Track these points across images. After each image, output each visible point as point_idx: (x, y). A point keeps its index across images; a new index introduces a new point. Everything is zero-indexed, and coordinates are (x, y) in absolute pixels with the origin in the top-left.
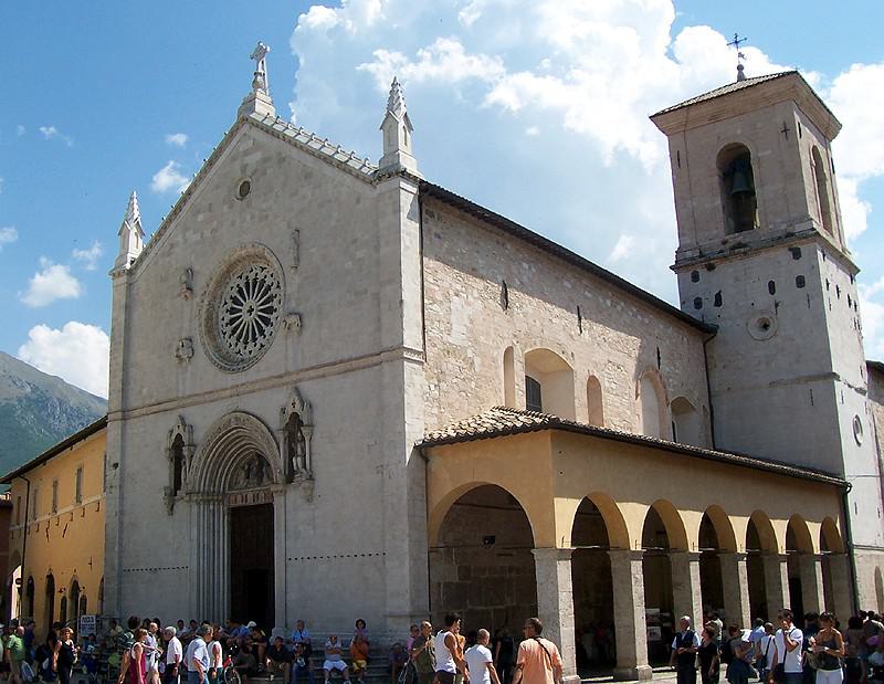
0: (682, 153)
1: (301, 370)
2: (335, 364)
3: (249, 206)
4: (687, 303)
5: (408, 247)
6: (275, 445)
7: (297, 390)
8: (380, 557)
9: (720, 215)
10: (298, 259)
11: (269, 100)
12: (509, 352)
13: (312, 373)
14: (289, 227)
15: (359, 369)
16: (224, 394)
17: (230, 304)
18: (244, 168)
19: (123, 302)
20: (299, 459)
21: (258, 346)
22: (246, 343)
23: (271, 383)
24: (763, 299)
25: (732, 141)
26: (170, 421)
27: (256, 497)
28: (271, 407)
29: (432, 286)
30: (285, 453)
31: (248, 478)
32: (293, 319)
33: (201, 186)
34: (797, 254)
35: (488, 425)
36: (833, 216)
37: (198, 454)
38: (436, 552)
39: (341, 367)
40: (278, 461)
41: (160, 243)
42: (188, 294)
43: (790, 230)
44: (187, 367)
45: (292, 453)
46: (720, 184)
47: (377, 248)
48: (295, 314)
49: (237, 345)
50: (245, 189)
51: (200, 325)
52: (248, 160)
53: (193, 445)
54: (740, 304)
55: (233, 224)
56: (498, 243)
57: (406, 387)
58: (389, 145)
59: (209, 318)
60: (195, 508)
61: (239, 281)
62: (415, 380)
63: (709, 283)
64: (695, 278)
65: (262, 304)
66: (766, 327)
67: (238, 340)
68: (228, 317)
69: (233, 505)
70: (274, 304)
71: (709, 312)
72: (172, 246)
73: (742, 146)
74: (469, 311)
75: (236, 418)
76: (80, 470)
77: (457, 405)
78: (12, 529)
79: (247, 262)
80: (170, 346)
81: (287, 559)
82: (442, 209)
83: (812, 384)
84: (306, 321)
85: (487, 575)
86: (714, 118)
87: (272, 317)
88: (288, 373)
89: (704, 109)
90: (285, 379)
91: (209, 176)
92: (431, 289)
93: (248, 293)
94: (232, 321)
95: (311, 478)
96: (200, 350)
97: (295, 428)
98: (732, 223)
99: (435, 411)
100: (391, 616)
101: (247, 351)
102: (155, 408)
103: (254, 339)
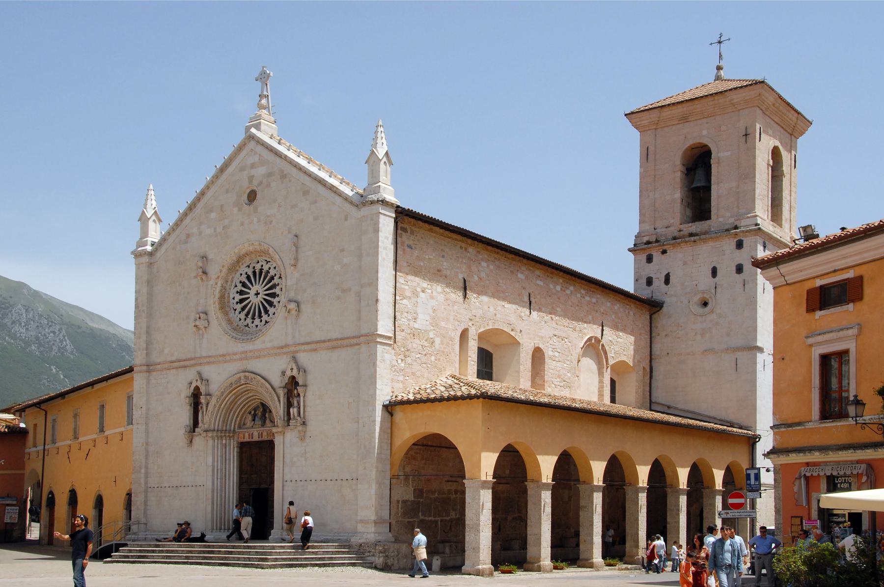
0: (651, 149)
1: (299, 344)
2: (324, 341)
3: (256, 211)
4: (640, 281)
5: (384, 259)
7: (294, 358)
8: (354, 482)
9: (678, 208)
10: (296, 259)
11: (272, 119)
12: (464, 334)
13: (306, 347)
14: (289, 232)
15: (343, 347)
17: (240, 287)
18: (251, 179)
20: (295, 410)
21: (263, 322)
22: (253, 318)
24: (705, 281)
25: (697, 141)
26: (190, 375)
29: (403, 286)
31: (254, 420)
33: (213, 189)
34: (740, 245)
35: (441, 391)
37: (213, 401)
38: (398, 479)
39: (330, 344)
40: (278, 409)
42: (204, 277)
43: (737, 223)
44: (203, 334)
45: (289, 405)
47: (360, 257)
48: (295, 302)
49: (245, 319)
50: (252, 196)
51: (214, 303)
52: (254, 172)
53: (209, 395)
54: (686, 284)
55: (242, 224)
56: (461, 247)
57: (378, 363)
59: (222, 297)
60: (210, 442)
61: (247, 270)
62: (385, 356)
63: (660, 266)
64: (650, 259)
65: (266, 290)
66: (705, 304)
67: (247, 315)
68: (238, 297)
69: (242, 440)
70: (277, 290)
71: (659, 290)
72: (188, 236)
73: (706, 146)
74: (433, 303)
76: (102, 407)
77: (418, 374)
78: (27, 450)
79: (253, 256)
80: (188, 317)
81: (284, 481)
82: (414, 225)
83: (739, 354)
84: (303, 307)
85: (436, 495)
86: (685, 119)
87: (275, 301)
88: (287, 346)
89: (679, 110)
90: (285, 350)
92: (401, 288)
94: (241, 301)
95: (304, 423)
96: (214, 323)
97: (293, 384)
98: (689, 213)
100: (361, 521)
101: (254, 325)
102: (176, 364)
103: (260, 316)
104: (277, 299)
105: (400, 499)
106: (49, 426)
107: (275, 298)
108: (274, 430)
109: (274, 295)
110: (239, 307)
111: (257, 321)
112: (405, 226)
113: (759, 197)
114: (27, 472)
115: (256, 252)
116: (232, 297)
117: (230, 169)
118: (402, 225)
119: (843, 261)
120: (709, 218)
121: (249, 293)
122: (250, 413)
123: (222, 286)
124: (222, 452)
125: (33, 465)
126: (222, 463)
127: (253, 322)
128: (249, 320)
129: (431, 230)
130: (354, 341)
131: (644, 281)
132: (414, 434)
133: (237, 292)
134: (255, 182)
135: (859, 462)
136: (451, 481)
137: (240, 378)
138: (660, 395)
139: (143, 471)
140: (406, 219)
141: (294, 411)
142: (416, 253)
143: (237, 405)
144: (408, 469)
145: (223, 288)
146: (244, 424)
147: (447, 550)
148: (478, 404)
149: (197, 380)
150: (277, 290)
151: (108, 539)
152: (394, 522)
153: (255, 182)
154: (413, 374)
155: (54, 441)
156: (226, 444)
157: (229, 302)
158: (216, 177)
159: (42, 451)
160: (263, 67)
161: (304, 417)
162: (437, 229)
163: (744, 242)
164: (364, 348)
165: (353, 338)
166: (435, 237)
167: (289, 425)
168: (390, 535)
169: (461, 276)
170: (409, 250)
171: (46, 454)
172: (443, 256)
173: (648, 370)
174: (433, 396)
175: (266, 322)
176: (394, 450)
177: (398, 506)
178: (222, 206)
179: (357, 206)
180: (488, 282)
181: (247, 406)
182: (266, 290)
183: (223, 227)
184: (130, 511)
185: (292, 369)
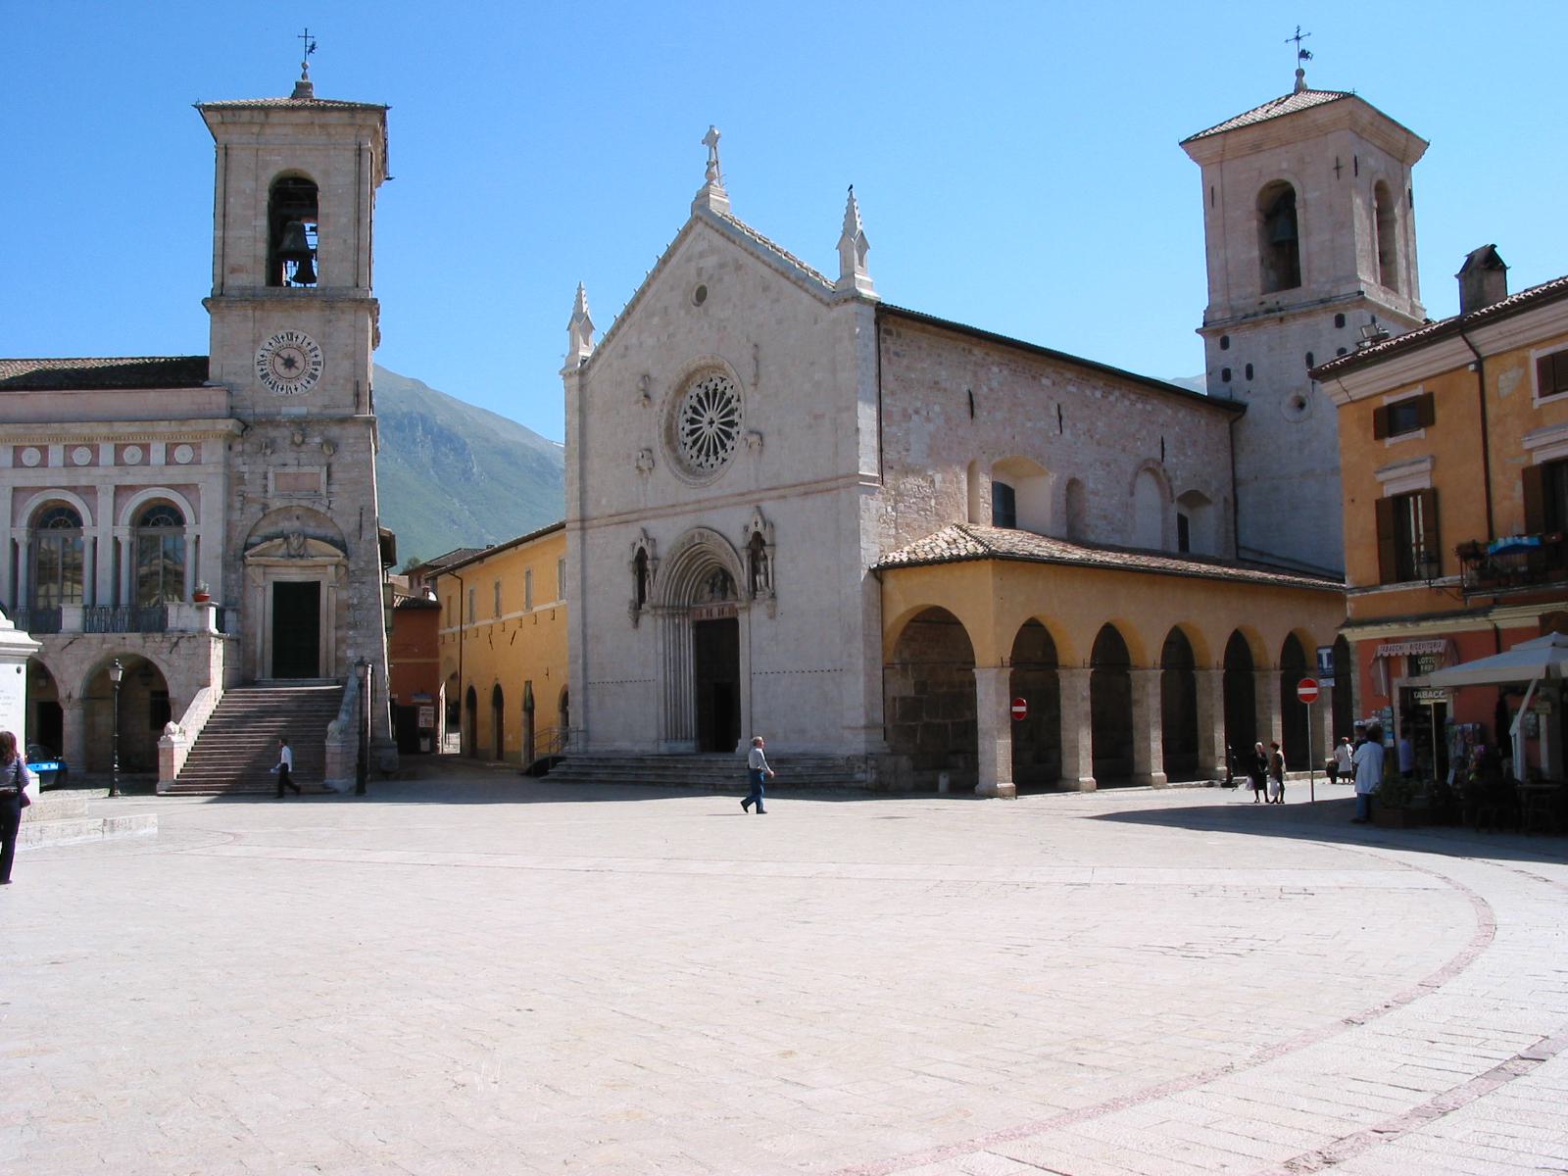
0: (1217, 189)
2: (795, 486)
3: (706, 311)
6: (737, 561)
9: (1256, 271)
10: (757, 376)
14: (748, 340)
15: (818, 492)
16: (687, 508)
17: (690, 414)
18: (700, 272)
19: (577, 404)
20: (762, 577)
21: (720, 459)
22: (708, 455)
23: (733, 500)
25: (1275, 177)
26: (633, 533)
27: (721, 612)
28: (735, 524)
30: (748, 569)
32: (754, 438)
33: (654, 288)
34: (1340, 322)
36: (1401, 262)
38: (893, 668)
40: (742, 577)
41: (613, 343)
44: (647, 478)
45: (755, 571)
46: (1259, 231)
49: (698, 457)
50: (701, 295)
51: (660, 436)
53: (655, 558)
56: (964, 349)
58: (845, 267)
60: (660, 622)
61: (698, 390)
64: (1225, 344)
68: (688, 427)
69: (698, 618)
70: (735, 418)
71: (1239, 384)
72: (626, 348)
75: (701, 534)
77: (915, 525)
78: (441, 632)
79: (705, 372)
80: (629, 456)
84: (767, 440)
85: (945, 689)
86: (1257, 148)
87: (733, 431)
88: (750, 492)
90: (748, 498)
91: (662, 276)
93: (714, 440)
94: (692, 432)
95: (773, 596)
96: (661, 464)
97: (757, 548)
98: (1273, 276)
99: (893, 532)
102: (616, 519)
103: (716, 453)
104: (736, 429)
105: (896, 695)
106: (466, 599)
107: (732, 427)
108: (737, 605)
109: (731, 424)
110: (689, 440)
111: (712, 459)
112: (889, 327)
113: (1362, 254)
114: (442, 660)
115: (708, 367)
116: (680, 427)
117: (674, 260)
118: (885, 326)
119: (1409, 374)
120: (1299, 285)
121: (700, 422)
122: (707, 582)
123: (669, 413)
124: (674, 635)
125: (448, 652)
126: (675, 649)
127: (707, 461)
128: (703, 458)
129: (923, 331)
130: (833, 484)
131: (1219, 375)
132: (910, 607)
133: (687, 421)
134: (705, 277)
135: (1440, 636)
136: (964, 670)
137: (693, 537)
138: (1248, 537)
139: (580, 661)
140: (891, 318)
141: (760, 579)
142: (905, 362)
143: (691, 571)
144: (906, 655)
145: (670, 416)
146: (701, 597)
147: (961, 764)
148: (987, 567)
149: (641, 540)
150: (735, 418)
151: (542, 751)
152: (890, 726)
153: (705, 277)
154: (908, 525)
155: (472, 620)
156: (679, 624)
157: (677, 434)
158: (658, 270)
159: (459, 634)
160: (711, 127)
161: (773, 588)
162: (930, 327)
163: (1346, 317)
164: (843, 493)
165: (830, 480)
166: (929, 339)
167: (755, 598)
168: (885, 744)
169: (965, 388)
170: (895, 358)
171: (463, 637)
172: (941, 363)
173: (1231, 500)
174: (930, 557)
175: (724, 460)
176: (886, 629)
177: (895, 705)
178: (666, 308)
179: (828, 305)
180: (1001, 394)
181: (703, 573)
182: (722, 417)
183: (669, 336)
184: (567, 714)
185: (756, 523)
